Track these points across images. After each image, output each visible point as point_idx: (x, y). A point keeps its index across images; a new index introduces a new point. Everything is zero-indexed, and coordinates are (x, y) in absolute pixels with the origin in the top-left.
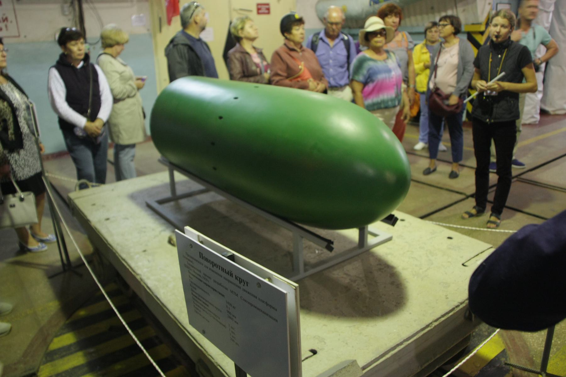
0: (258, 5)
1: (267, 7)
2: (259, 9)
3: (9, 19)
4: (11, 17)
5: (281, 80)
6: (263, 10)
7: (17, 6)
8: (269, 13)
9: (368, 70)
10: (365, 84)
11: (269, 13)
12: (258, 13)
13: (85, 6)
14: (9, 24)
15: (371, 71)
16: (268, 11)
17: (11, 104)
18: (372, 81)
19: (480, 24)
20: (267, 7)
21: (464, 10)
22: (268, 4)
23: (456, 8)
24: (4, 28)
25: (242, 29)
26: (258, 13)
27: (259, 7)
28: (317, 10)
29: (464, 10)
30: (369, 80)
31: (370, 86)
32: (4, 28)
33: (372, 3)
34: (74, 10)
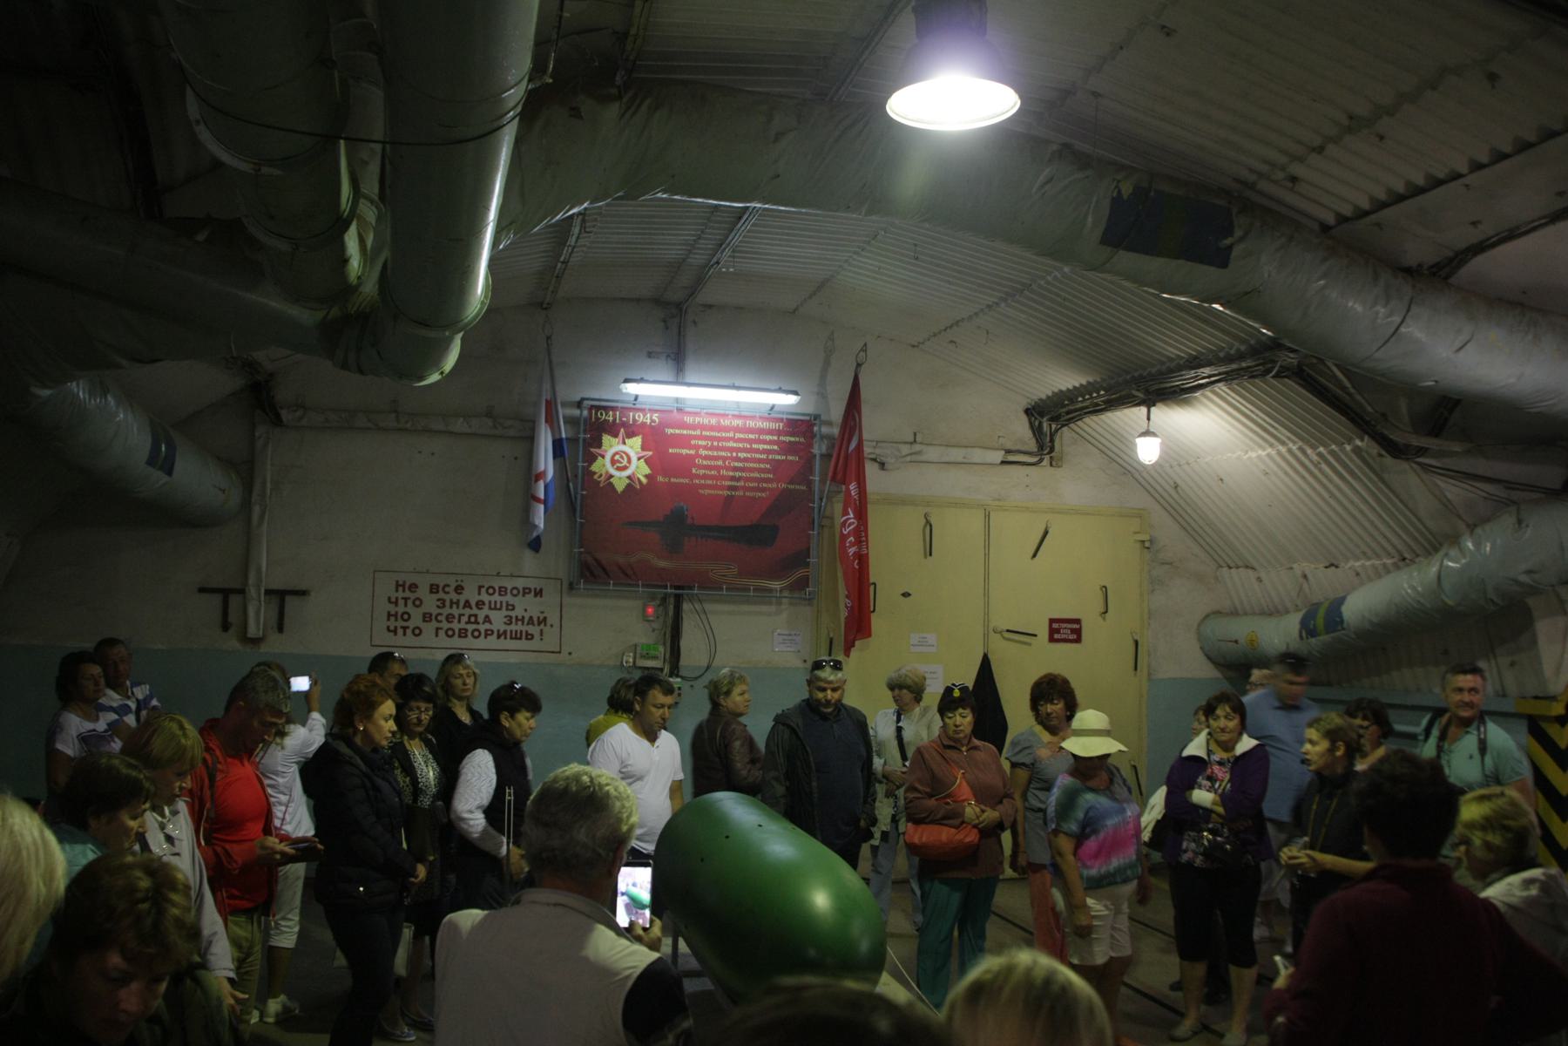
0: (1052, 621)
1: (1075, 626)
2: (1052, 632)
3: (549, 622)
4: (553, 619)
5: (918, 798)
6: (1066, 633)
7: (567, 600)
8: (1078, 640)
9: (1087, 813)
10: (1080, 839)
11: (1078, 640)
12: (1052, 640)
13: (686, 606)
14: (547, 629)
15: (1091, 814)
16: (1077, 636)
17: (415, 781)
18: (1095, 832)
19: (1553, 698)
20: (1075, 626)
21: (1512, 664)
22: (1078, 621)
23: (1495, 657)
24: (537, 637)
25: (728, 693)
26: (1052, 640)
27: (1055, 626)
28: (1200, 637)
29: (1512, 664)
30: (1088, 830)
31: (1091, 844)
32: (537, 637)
33: (1304, 635)
34: (666, 613)
